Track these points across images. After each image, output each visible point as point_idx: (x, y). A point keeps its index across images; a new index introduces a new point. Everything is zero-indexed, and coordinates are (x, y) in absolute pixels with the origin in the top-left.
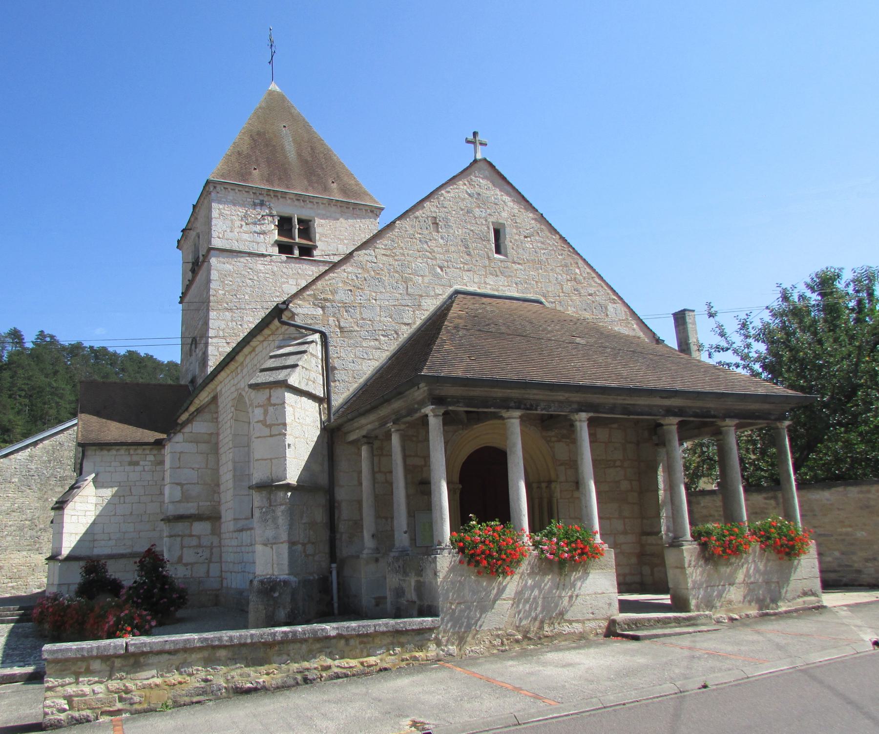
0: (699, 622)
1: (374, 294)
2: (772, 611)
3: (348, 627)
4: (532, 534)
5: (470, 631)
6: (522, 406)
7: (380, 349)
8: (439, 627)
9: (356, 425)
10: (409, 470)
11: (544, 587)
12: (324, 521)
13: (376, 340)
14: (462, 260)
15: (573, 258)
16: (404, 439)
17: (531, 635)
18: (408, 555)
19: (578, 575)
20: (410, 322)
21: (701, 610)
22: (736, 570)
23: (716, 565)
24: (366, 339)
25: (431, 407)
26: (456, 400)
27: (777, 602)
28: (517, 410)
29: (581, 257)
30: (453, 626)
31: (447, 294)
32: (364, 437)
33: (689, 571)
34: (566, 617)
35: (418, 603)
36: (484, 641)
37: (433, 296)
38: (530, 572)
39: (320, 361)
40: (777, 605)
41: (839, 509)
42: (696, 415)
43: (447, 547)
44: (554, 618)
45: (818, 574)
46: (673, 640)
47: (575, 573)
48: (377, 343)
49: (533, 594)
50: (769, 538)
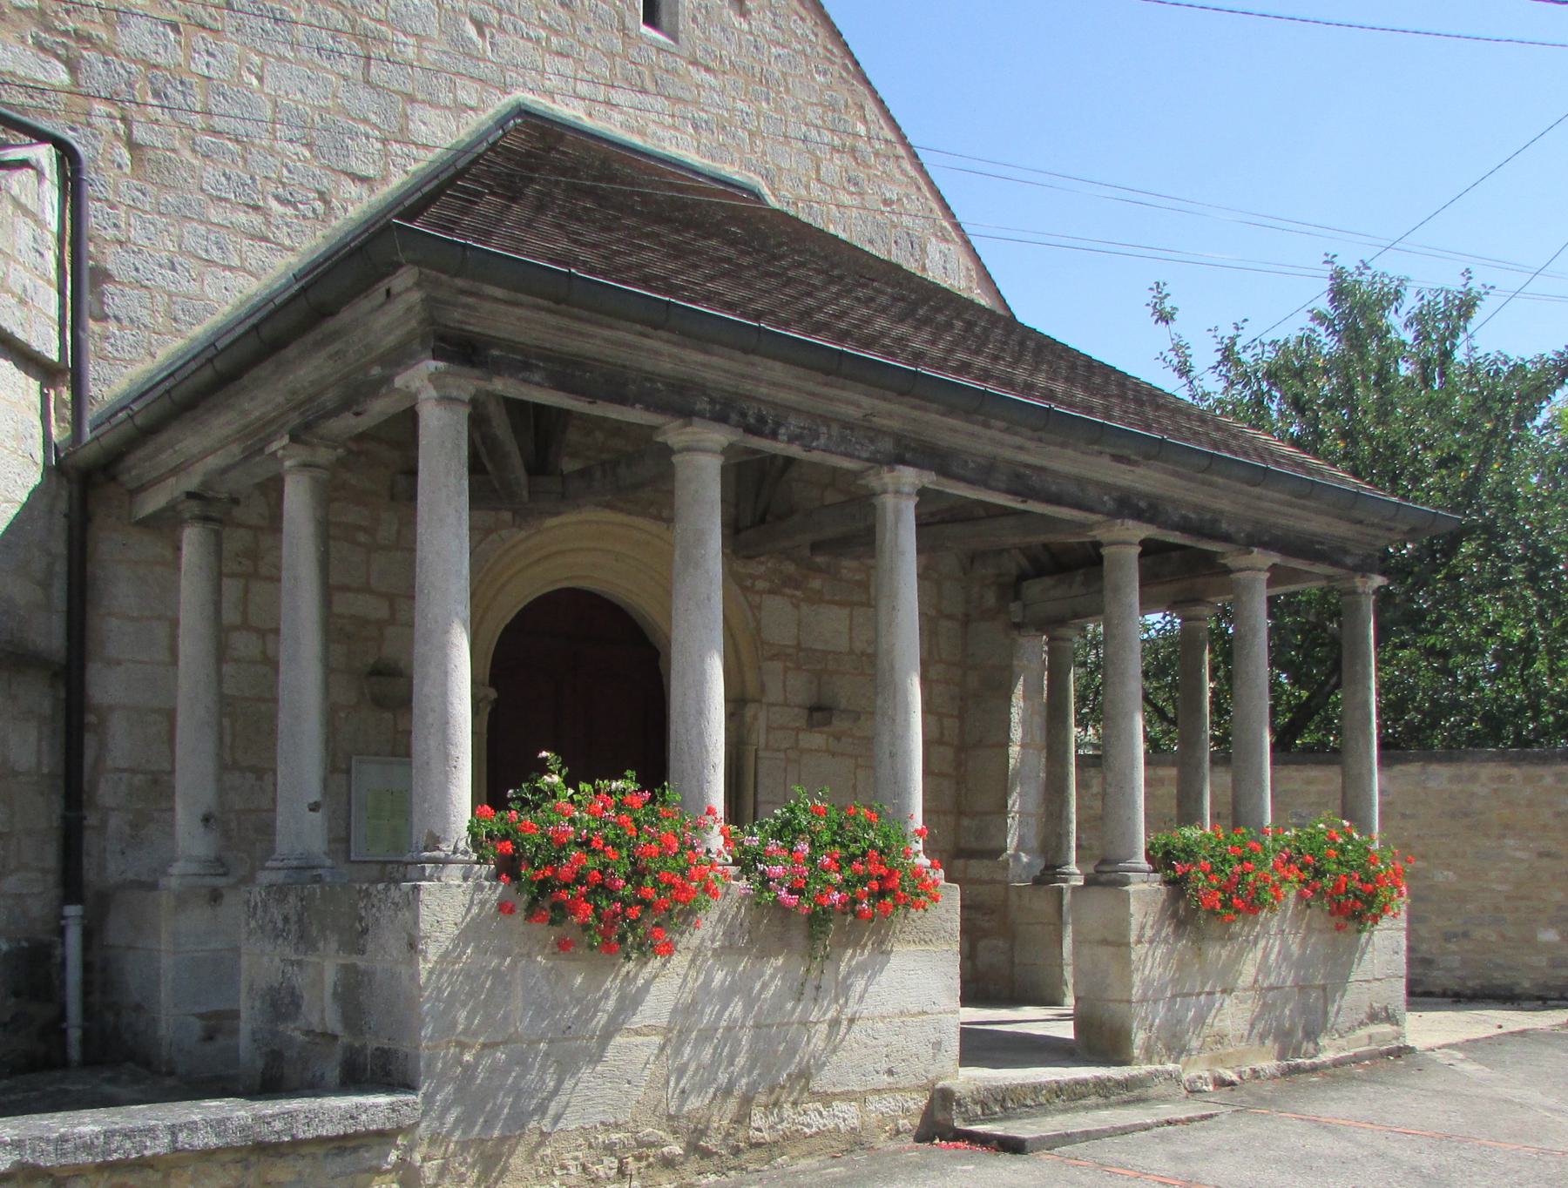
0: (1152, 1092)
1: (257, 60)
2: (1308, 1062)
3: (63, 1139)
4: (733, 828)
5: (521, 1136)
6: (734, 417)
7: (266, 239)
8: (417, 1124)
9: (167, 459)
10: (334, 629)
11: (760, 993)
12: (45, 770)
13: (256, 208)
14: (543, 15)
15: (852, 91)
16: (328, 495)
17: (711, 1142)
18: (318, 879)
19: (858, 958)
20: (371, 173)
21: (1156, 1058)
22: (1240, 954)
23: (1200, 938)
24: (221, 199)
25: (432, 365)
26: (521, 361)
27: (1317, 1036)
28: (717, 426)
29: (874, 93)
30: (466, 1121)
31: (491, 111)
32: (190, 495)
33: (1137, 952)
34: (815, 1085)
35: (345, 1038)
36: (563, 1167)
37: (447, 107)
38: (722, 947)
39: (52, 242)
40: (1317, 1044)
41: (1404, 816)
42: (1185, 527)
43: (460, 856)
44: (783, 1087)
45: (1403, 970)
46: (1109, 1150)
47: (850, 951)
48: (257, 219)
49: (727, 1014)
50: (1319, 873)
